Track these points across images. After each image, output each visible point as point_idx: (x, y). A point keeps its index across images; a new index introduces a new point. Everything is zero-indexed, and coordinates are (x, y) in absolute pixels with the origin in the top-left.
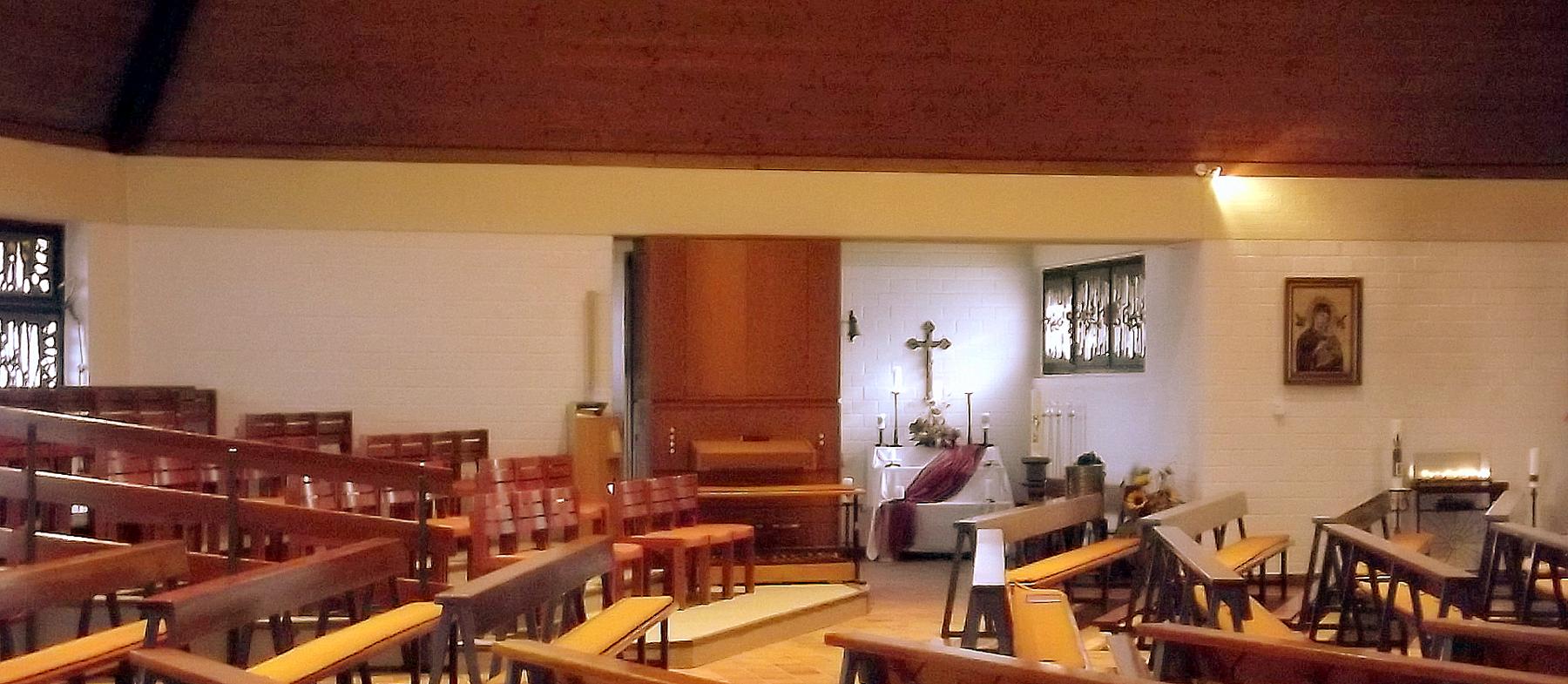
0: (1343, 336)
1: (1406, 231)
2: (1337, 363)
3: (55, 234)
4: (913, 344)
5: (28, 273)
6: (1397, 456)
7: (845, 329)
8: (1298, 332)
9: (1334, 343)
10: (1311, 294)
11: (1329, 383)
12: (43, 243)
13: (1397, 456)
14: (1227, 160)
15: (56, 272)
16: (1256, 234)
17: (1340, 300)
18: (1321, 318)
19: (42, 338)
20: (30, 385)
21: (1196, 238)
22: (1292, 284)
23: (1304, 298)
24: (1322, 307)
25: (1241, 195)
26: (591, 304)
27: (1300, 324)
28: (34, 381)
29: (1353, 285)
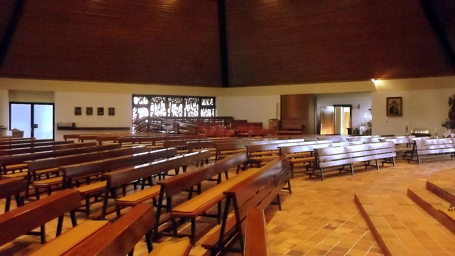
0: (399, 108)
1: (412, 88)
2: (398, 112)
3: (214, 99)
4: (370, 109)
5: (209, 102)
6: (407, 129)
7: (105, 121)
8: (390, 107)
9: (397, 109)
10: (392, 100)
11: (397, 116)
12: (212, 99)
13: (407, 129)
14: (376, 78)
15: (214, 102)
16: (382, 89)
17: (398, 101)
18: (394, 104)
19: (212, 111)
20: (38, 136)
21: (372, 90)
22: (388, 99)
23: (391, 101)
24: (394, 102)
25: (378, 83)
26: (277, 105)
27: (390, 105)
28: (210, 116)
29: (400, 98)
